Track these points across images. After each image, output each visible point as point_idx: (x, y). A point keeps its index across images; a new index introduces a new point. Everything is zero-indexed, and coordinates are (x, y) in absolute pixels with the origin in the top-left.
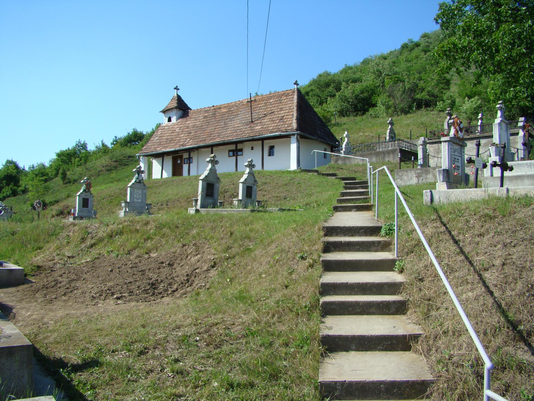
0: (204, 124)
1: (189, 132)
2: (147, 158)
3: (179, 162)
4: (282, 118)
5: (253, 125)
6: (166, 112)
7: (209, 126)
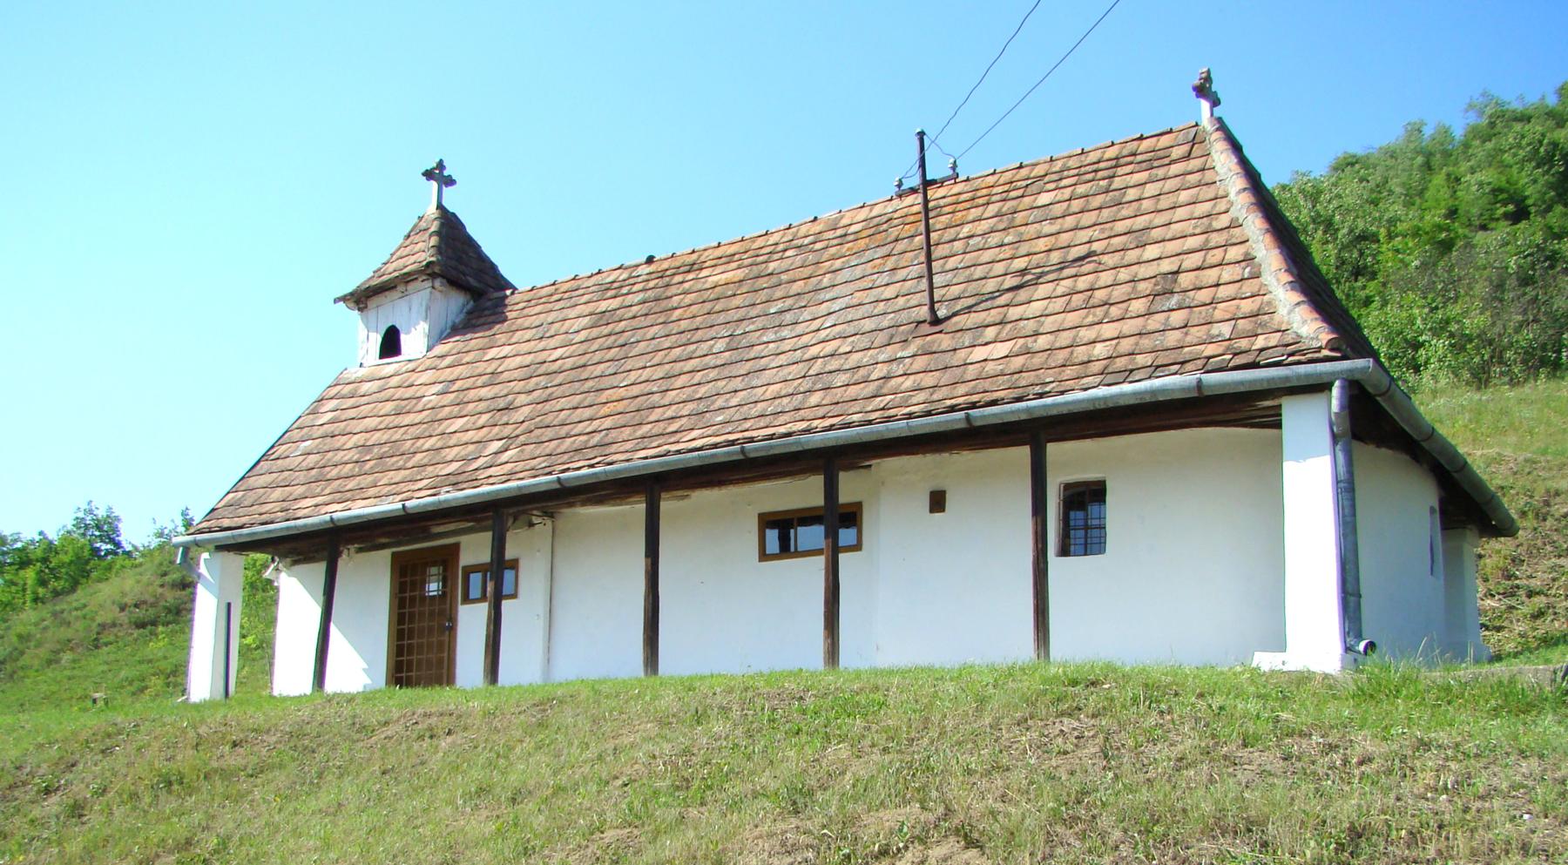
0: (598, 357)
1: (502, 403)
2: (237, 561)
3: (433, 588)
4: (1167, 285)
5: (945, 341)
6: (372, 303)
7: (629, 364)
